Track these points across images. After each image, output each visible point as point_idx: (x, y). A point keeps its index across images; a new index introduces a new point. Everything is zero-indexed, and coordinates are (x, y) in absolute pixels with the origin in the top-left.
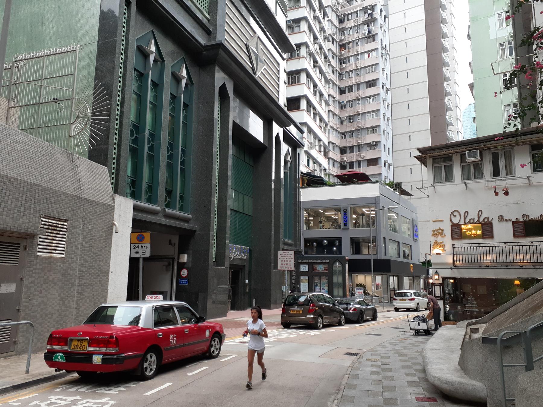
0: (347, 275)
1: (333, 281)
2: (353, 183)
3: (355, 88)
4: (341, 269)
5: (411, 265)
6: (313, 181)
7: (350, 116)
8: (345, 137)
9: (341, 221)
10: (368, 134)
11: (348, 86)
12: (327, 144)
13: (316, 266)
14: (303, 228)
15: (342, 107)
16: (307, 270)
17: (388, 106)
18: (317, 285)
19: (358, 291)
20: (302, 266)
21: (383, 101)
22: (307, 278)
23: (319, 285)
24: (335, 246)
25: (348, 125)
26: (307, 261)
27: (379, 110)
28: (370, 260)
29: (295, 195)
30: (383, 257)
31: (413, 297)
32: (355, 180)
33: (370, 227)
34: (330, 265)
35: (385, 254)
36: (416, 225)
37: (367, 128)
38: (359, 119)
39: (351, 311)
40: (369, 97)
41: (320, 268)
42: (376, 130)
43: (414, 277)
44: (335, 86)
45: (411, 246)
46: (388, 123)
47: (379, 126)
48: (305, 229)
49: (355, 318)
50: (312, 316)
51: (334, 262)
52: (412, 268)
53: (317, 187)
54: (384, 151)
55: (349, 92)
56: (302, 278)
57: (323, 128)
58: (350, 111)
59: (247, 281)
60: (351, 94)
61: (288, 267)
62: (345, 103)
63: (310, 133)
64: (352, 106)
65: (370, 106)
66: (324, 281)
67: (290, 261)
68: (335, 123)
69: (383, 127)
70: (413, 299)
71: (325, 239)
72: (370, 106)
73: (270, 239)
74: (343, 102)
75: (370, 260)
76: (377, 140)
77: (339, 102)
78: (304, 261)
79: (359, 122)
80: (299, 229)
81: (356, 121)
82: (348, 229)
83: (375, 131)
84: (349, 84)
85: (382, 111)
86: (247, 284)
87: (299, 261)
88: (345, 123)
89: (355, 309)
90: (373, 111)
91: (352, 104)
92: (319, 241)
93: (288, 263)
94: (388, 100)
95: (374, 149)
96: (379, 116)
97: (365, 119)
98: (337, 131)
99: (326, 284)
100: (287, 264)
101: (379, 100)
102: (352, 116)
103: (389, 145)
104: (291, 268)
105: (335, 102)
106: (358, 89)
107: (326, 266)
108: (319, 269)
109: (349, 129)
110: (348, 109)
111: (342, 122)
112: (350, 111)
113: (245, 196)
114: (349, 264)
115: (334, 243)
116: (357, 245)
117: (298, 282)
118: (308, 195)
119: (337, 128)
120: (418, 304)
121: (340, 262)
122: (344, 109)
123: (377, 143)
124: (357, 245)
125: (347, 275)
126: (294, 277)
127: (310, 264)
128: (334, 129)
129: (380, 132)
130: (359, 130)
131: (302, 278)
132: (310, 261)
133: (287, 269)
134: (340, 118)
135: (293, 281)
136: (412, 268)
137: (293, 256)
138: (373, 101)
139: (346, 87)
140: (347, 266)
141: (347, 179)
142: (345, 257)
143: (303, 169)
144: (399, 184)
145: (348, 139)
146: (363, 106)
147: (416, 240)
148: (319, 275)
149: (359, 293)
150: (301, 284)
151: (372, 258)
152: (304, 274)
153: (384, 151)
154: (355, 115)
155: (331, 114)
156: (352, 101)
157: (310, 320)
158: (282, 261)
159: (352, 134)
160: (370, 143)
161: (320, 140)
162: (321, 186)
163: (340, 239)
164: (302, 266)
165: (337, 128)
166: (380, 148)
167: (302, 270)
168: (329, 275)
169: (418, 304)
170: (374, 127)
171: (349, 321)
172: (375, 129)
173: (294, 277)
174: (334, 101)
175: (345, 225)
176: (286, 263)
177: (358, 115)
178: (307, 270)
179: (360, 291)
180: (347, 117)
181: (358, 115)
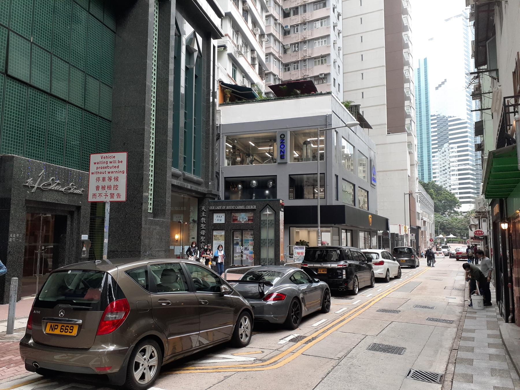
0: (282, 227)
1: (260, 236)
3: (300, 10)
4: (272, 218)
5: (370, 216)
6: (239, 95)
7: (295, 44)
8: (289, 70)
9: (277, 155)
10: (315, 65)
11: (293, 8)
12: (263, 58)
13: (237, 215)
14: (223, 163)
15: (286, 33)
16: (223, 221)
17: (339, 34)
18: (237, 244)
19: (297, 251)
20: (215, 215)
21: (334, 27)
22: (223, 233)
24: (267, 188)
25: (293, 54)
26: (224, 208)
27: (328, 36)
28: (316, 207)
30: (334, 203)
31: (381, 259)
32: (298, 92)
33: (317, 160)
34: (257, 213)
35: (337, 199)
36: (373, 166)
37: (315, 58)
38: (305, 47)
39: (271, 302)
40: (317, 20)
41: (243, 218)
42: (325, 60)
43: (371, 233)
44: (277, 6)
45: (368, 192)
46: (339, 54)
47: (329, 55)
48: (226, 165)
49: (281, 320)
50: (112, 348)
51: (263, 209)
52: (370, 220)
53: (243, 103)
54: (334, 86)
55: (294, 15)
56: (215, 233)
57: (257, 36)
58: (295, 37)
59: (85, 237)
60: (296, 17)
61: (112, 195)
62: (289, 27)
63: (237, 34)
64: (297, 31)
65: (318, 30)
66: (249, 237)
67: (116, 179)
68: (278, 51)
69: (333, 57)
70: (382, 263)
71: (254, 178)
72: (318, 30)
74: (287, 26)
75: (316, 207)
76: (326, 72)
77: (282, 26)
78: (219, 208)
79: (306, 50)
81: (301, 49)
82: (286, 163)
83: (324, 61)
84: (294, 5)
85: (333, 38)
86: (83, 242)
87: (212, 208)
88: (289, 52)
89: (280, 297)
90: (322, 38)
91: (297, 29)
92: (245, 182)
93: (113, 183)
94: (339, 27)
95: (323, 83)
96: (329, 42)
97: (312, 47)
98: (279, 61)
99: (250, 242)
100: (109, 187)
101: (329, 24)
102: (298, 43)
103: (340, 80)
104: (119, 195)
105: (278, 25)
106: (305, 11)
107: (251, 215)
108: (241, 220)
109: (294, 60)
110: (292, 35)
111: (285, 51)
112: (295, 37)
113: (90, 80)
114: (285, 211)
115: (267, 183)
116: (297, 187)
118: (231, 116)
119: (279, 56)
120: (388, 269)
121: (272, 209)
122: (288, 36)
123: (327, 75)
124: (297, 187)
125: (282, 227)
126: (203, 232)
127: (228, 213)
128: (276, 58)
129: (330, 62)
130: (305, 60)
132: (228, 208)
133: (108, 199)
134: (283, 46)
135: (202, 238)
136: (370, 220)
137: (123, 167)
138: (322, 25)
139: (290, 9)
140: (282, 214)
141: (284, 91)
142: (279, 200)
144: (357, 107)
145: (292, 71)
146: (310, 31)
147: (373, 186)
148: (242, 229)
149: (298, 253)
151: (319, 203)
152: (219, 227)
153: (334, 86)
154: (301, 42)
155: (272, 39)
156: (297, 25)
157: (105, 362)
158: (98, 179)
159: (297, 66)
160: (318, 76)
161: (253, 50)
162: (249, 102)
163: (274, 179)
164: (215, 215)
165: (279, 56)
166: (330, 82)
167: (215, 221)
168: (255, 227)
169: (388, 269)
170: (322, 57)
171: (264, 326)
172: (323, 58)
173: (203, 232)
174: (276, 24)
175: (282, 157)
176: (107, 183)
177: (304, 42)
178: (223, 221)
179: (300, 251)
180: (291, 44)
181: (304, 42)
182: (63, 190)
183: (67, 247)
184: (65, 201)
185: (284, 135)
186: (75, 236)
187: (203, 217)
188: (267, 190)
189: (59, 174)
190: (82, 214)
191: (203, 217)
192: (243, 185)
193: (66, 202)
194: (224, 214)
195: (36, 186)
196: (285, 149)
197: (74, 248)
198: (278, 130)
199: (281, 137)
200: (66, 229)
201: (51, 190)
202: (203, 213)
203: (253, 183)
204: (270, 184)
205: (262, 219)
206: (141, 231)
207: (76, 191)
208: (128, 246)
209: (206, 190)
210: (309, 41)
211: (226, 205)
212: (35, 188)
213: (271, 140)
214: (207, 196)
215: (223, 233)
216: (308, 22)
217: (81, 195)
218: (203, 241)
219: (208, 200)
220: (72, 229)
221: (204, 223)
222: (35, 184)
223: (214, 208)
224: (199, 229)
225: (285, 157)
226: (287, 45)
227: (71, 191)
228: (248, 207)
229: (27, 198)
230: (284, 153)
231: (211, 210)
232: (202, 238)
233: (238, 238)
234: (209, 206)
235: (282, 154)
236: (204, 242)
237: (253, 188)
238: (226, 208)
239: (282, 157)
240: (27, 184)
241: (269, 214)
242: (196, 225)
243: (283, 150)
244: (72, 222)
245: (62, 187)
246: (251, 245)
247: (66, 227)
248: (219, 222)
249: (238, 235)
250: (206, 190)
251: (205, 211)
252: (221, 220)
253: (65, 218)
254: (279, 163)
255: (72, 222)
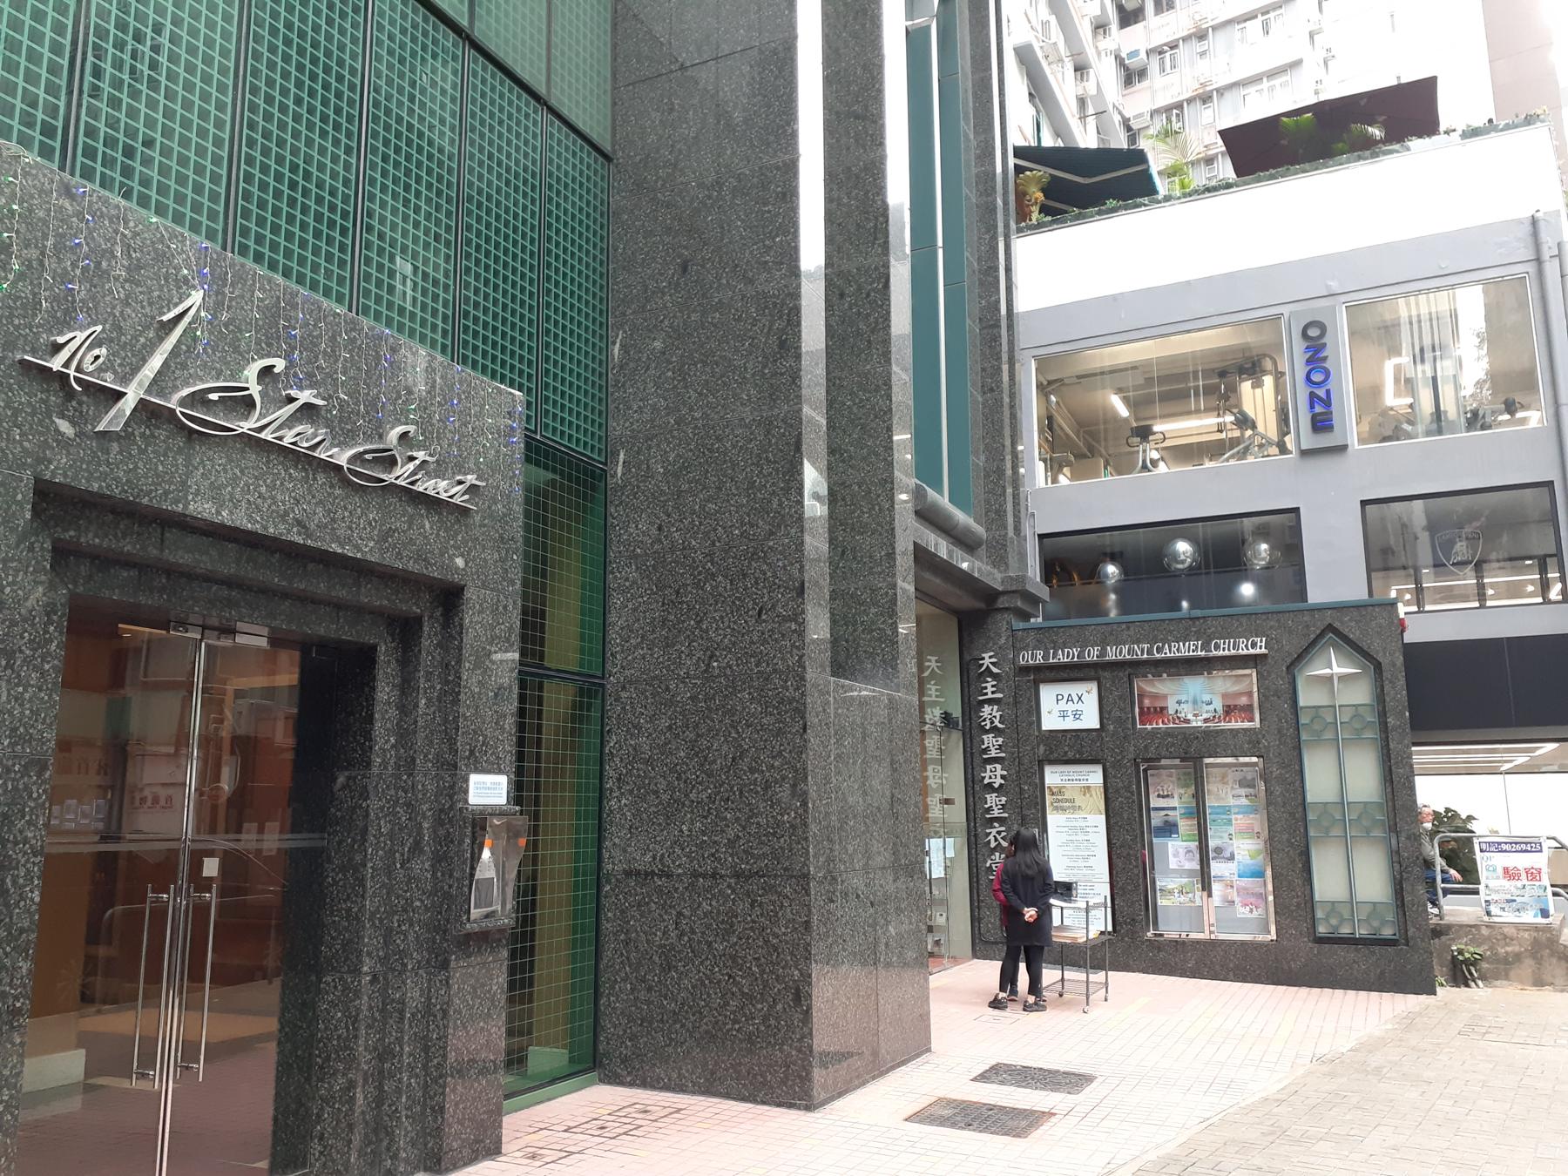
2: (1365, 148)
6: (1091, 182)
16: (1091, 720)
18: (1169, 829)
20: (1049, 695)
22: (1094, 776)
23: (1186, 826)
26: (1092, 654)
29: (986, 279)
40: (1251, 16)
41: (1193, 702)
48: (1043, 484)
56: (1053, 776)
59: (488, 789)
60: (1167, 17)
62: (1143, 55)
73: (788, 344)
80: (1016, 481)
82: (1343, 448)
86: (479, 822)
87: (1027, 658)
90: (1272, 74)
102: (1179, 106)
108: (1187, 711)
110: (1155, 79)
117: (1030, 807)
118: (1054, 270)
122: (1138, 86)
126: (994, 775)
131: (1053, 776)
132: (1112, 654)
135: (991, 799)
143: (1020, 123)
149: (1510, 874)
150: (1053, 819)
152: (1072, 748)
154: (1189, 101)
163: (1285, 530)
164: (1049, 695)
173: (994, 775)
175: (1321, 424)
178: (1091, 720)
180: (1154, 113)
182: (343, 458)
183: (374, 856)
184: (357, 535)
185: (1323, 328)
186: (426, 781)
187: (990, 702)
188: (1246, 579)
189: (310, 344)
190: (468, 639)
191: (990, 702)
192: (1125, 570)
193: (366, 549)
194: (1093, 687)
195: (133, 395)
196: (1331, 385)
197: (421, 866)
198: (1285, 310)
199: (1305, 335)
200: (368, 736)
201: (248, 440)
202: (989, 686)
203: (1175, 557)
204: (1256, 554)
205: (1302, 703)
206: (802, 750)
207: (428, 486)
208: (731, 843)
209: (999, 576)
210: (1221, 91)
211: (1104, 644)
212: (128, 404)
213: (1223, 377)
214: (1002, 602)
215: (1094, 776)
216: (1214, 28)
217: (464, 511)
218: (996, 813)
219: (1003, 625)
220: (404, 736)
221: (994, 729)
222: (125, 379)
223: (1039, 660)
224: (974, 761)
225: (1336, 422)
226: (1141, 115)
227: (401, 474)
228: (1225, 649)
229: (59, 469)
230: (1327, 402)
231: (1026, 670)
232: (991, 799)
233: (1174, 802)
234: (1017, 650)
235: (1318, 409)
236: (1001, 820)
237: (1176, 575)
238: (1103, 653)
239: (1321, 424)
240: (56, 364)
241: (1342, 678)
242: (956, 739)
243: (1321, 393)
244: (406, 686)
245: (344, 437)
246: (1248, 832)
247: (370, 719)
248: (1070, 724)
249: (1170, 786)
250: (999, 576)
251: (995, 676)
252: (1077, 716)
253: (365, 657)
254: (1304, 453)
255: (406, 686)
